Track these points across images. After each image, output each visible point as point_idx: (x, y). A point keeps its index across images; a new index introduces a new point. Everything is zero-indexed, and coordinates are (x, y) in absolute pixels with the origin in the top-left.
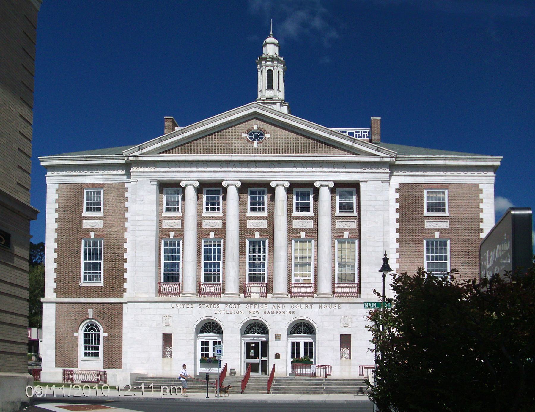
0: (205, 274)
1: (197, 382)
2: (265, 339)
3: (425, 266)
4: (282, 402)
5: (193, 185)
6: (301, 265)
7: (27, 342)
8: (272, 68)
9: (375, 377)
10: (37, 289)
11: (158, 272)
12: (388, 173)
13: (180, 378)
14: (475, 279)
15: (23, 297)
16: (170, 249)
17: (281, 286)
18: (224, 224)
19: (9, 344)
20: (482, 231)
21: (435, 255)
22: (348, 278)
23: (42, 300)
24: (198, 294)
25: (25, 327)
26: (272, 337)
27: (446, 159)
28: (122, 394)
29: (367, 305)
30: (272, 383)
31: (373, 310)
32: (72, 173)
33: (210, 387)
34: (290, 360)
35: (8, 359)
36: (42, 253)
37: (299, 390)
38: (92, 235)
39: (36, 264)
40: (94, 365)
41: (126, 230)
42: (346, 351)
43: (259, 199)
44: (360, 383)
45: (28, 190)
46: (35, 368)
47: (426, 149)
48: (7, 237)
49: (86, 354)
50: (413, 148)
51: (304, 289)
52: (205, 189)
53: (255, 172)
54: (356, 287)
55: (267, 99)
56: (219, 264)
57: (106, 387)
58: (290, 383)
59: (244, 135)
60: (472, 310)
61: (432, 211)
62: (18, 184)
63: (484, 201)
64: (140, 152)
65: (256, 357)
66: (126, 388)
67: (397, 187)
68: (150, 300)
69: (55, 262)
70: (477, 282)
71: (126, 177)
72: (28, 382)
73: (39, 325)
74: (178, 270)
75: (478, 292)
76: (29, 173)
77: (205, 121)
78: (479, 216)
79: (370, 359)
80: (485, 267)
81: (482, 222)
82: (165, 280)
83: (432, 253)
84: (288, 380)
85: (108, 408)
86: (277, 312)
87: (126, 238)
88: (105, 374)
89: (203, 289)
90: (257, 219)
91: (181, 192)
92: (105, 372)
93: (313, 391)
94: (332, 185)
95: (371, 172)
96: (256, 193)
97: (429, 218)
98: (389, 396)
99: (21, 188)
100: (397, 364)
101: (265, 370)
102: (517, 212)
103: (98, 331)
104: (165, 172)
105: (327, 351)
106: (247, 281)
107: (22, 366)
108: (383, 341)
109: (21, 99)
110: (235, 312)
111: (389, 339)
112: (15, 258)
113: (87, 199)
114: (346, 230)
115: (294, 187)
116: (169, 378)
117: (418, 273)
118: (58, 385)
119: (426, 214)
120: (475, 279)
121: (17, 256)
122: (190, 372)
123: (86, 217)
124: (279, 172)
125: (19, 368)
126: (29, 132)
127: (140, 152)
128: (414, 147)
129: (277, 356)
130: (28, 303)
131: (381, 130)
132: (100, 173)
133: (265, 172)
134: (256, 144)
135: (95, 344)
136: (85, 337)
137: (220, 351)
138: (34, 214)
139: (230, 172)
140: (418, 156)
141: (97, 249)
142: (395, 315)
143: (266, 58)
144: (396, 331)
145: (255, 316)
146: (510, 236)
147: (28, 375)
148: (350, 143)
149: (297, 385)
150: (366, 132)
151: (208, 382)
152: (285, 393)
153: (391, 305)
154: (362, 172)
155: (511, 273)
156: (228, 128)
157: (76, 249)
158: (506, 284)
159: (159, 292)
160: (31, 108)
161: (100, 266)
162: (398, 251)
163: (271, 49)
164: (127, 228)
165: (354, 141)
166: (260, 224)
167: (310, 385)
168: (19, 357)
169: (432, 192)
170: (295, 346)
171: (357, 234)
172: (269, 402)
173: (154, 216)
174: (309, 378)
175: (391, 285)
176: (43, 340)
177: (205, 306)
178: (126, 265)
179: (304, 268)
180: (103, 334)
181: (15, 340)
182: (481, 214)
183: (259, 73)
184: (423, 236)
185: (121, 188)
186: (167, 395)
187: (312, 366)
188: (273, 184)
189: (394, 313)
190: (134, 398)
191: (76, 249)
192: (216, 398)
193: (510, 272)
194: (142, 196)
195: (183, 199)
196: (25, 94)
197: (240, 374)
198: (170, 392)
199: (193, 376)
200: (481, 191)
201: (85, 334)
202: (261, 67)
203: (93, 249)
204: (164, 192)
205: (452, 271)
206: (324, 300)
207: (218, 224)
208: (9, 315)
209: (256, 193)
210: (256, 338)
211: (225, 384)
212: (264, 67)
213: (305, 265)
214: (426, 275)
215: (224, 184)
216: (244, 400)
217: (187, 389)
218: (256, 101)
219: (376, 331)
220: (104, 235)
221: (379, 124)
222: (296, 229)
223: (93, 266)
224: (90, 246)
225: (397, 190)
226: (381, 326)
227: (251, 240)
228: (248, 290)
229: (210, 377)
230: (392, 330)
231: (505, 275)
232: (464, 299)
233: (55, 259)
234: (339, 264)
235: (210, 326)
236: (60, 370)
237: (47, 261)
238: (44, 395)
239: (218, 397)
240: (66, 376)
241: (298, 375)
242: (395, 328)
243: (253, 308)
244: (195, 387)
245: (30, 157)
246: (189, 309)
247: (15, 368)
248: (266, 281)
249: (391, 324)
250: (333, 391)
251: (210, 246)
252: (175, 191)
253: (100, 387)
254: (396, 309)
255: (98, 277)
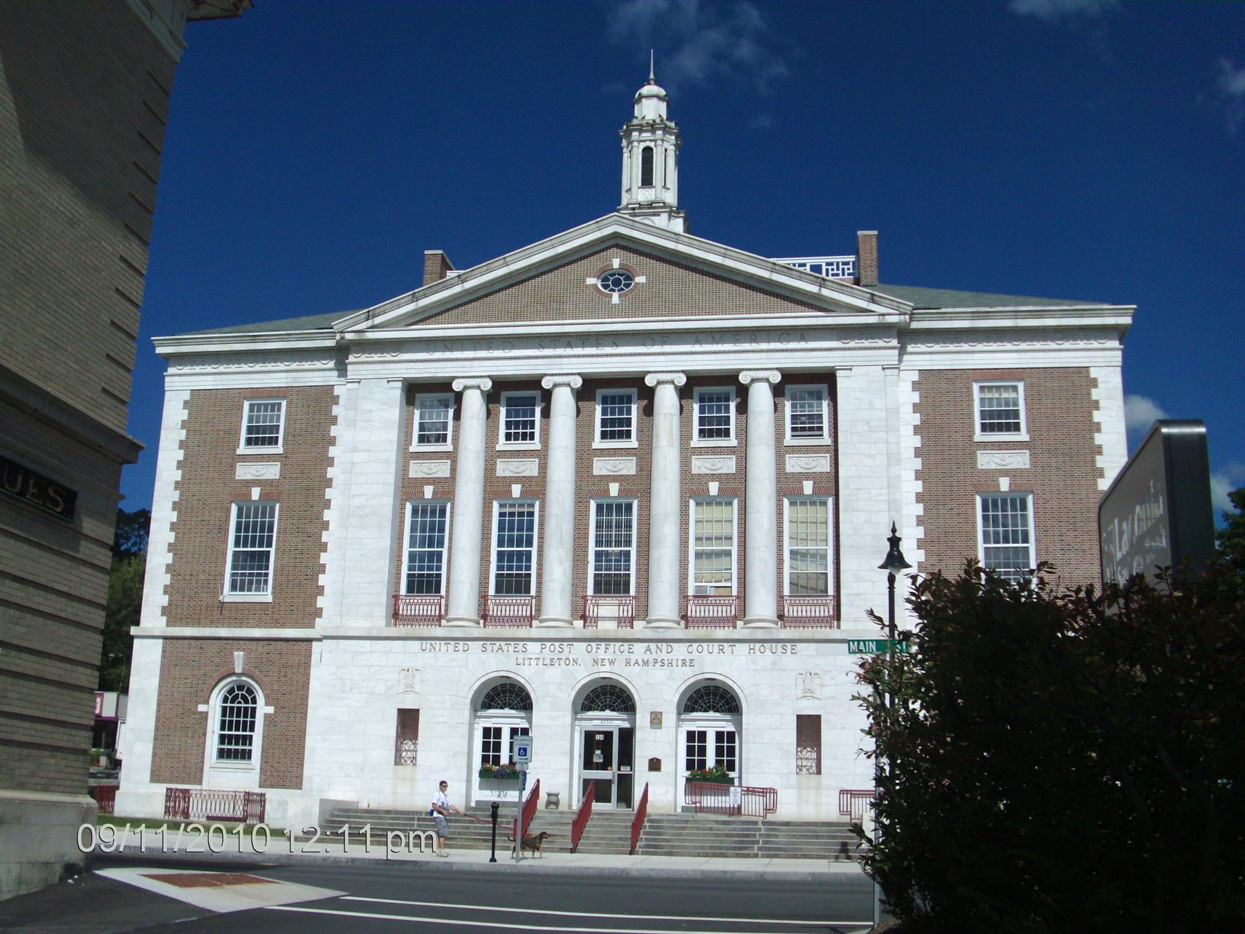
0: (498, 576)
1: (472, 822)
2: (626, 725)
3: (981, 556)
4: (663, 875)
5: (479, 387)
6: (709, 555)
7: (92, 723)
8: (652, 145)
9: (877, 817)
10: (126, 608)
11: (394, 572)
12: (894, 348)
13: (431, 813)
14: (1091, 585)
15: (92, 623)
16: (424, 524)
17: (664, 603)
18: (543, 468)
19: (49, 728)
20: (1101, 473)
21: (1001, 529)
22: (812, 584)
23: (134, 630)
24: (482, 621)
25: (91, 691)
26: (642, 718)
27: (1016, 315)
28: (298, 849)
29: (856, 646)
30: (640, 829)
31: (869, 658)
32: (222, 369)
33: (501, 835)
34: (683, 773)
35: (44, 761)
36: (142, 532)
37: (702, 848)
38: (256, 493)
39: (128, 554)
40: (240, 778)
41: (329, 483)
42: (809, 754)
43: (621, 413)
44: (842, 831)
45: (124, 403)
46: (105, 782)
47: (974, 294)
48: (70, 497)
49: (222, 754)
50: (949, 294)
51: (715, 610)
52: (697, 390)
53: (612, 355)
54: (832, 604)
55: (641, 206)
56: (529, 554)
57: (262, 832)
58: (683, 828)
59: (591, 281)
60: (1088, 660)
61: (992, 430)
62: (104, 390)
63: (1102, 404)
64: (369, 323)
65: (606, 765)
66: (308, 835)
67: (916, 378)
68: (374, 634)
69: (169, 551)
70: (1097, 594)
71: (336, 373)
72: (85, 815)
73: (121, 686)
74: (439, 568)
75: (1100, 615)
76: (129, 370)
77: (510, 256)
78: (1092, 438)
79: (863, 774)
80: (1111, 556)
81: (1100, 453)
82: (410, 589)
83: (996, 524)
84: (677, 821)
85: (263, 881)
86: (656, 661)
87: (329, 501)
88: (262, 799)
89: (493, 610)
90: (615, 455)
91: (452, 401)
92: (263, 795)
93: (735, 848)
94: (776, 378)
95: (860, 349)
96: (613, 399)
97: (985, 445)
98: (910, 864)
99: (108, 398)
100: (926, 787)
101: (625, 797)
102: (1175, 430)
103: (254, 701)
104: (422, 361)
105: (767, 756)
106: (590, 591)
107: (74, 777)
108: (893, 732)
109: (127, 226)
110: (562, 662)
111: (905, 727)
112: (83, 542)
113: (250, 420)
114: (807, 476)
115: (694, 386)
116: (408, 813)
117: (966, 572)
118: (153, 824)
119: (979, 436)
120: (1091, 585)
121: (88, 538)
122: (455, 799)
123: (245, 458)
124: (663, 354)
125: (68, 783)
126: (136, 289)
127: (369, 323)
128: (950, 292)
129: (655, 765)
130: (101, 638)
131: (880, 258)
132: (281, 366)
133: (635, 355)
134: (616, 298)
135: (244, 730)
136: (224, 715)
137: (525, 750)
138: (136, 452)
139: (560, 357)
140: (957, 310)
141: (263, 523)
142: (919, 671)
143: (641, 125)
144: (922, 707)
145: (605, 671)
146: (1162, 484)
147: (87, 800)
148: (813, 289)
149: (698, 835)
150: (847, 263)
151: (494, 822)
152: (670, 854)
153: (908, 646)
154: (840, 349)
155: (1170, 572)
156: (558, 268)
157: (217, 522)
158: (1161, 597)
159: (396, 615)
160: (144, 242)
161: (268, 560)
162: (920, 521)
163: (651, 106)
164: (331, 480)
165: (823, 283)
166: (622, 466)
167: (727, 835)
168: (71, 757)
169: (990, 388)
170: (696, 740)
171: (830, 485)
172: (635, 873)
173: (391, 454)
174: (726, 818)
175: (908, 601)
176: (129, 719)
177: (496, 648)
178: (324, 558)
179: (716, 563)
180: (263, 709)
181: (64, 718)
182: (1096, 435)
183: (626, 156)
184: (975, 486)
185: (326, 396)
186: (402, 853)
187: (732, 789)
188: (650, 381)
189: (915, 666)
190: (324, 859)
191: (217, 522)
192: (513, 862)
193: (1167, 568)
194: (370, 411)
195: (457, 416)
196: (133, 215)
197: (570, 806)
198: (408, 845)
199: (462, 809)
200: (1094, 383)
201: (224, 709)
202: (630, 143)
203: (255, 523)
204: (417, 402)
205: (1041, 565)
206: (759, 635)
207: (530, 468)
208: (58, 664)
209: (613, 399)
210: (608, 721)
211: (535, 829)
212: (635, 144)
213: (719, 554)
214: (983, 575)
215: (546, 383)
216: (576, 868)
217: (446, 838)
218: (618, 211)
219: (875, 708)
220: (280, 494)
221: (874, 244)
222: (700, 475)
223: (253, 560)
224: (248, 516)
225: (916, 386)
226: (887, 695)
227: (600, 501)
228: (591, 611)
229: (501, 811)
230: (911, 707)
231: (1158, 576)
232: (1071, 634)
233: (170, 545)
234: (792, 553)
235: (506, 694)
236: (161, 789)
237: (151, 549)
238: (118, 847)
239: (518, 859)
240: (172, 804)
241: (702, 810)
242: (919, 701)
243: (601, 651)
244: (465, 834)
245: (133, 338)
246: (461, 655)
247: (58, 782)
248: (633, 592)
249: (910, 691)
250: (780, 849)
251: (512, 514)
252: (439, 401)
253: (248, 831)
254: (920, 657)
255: (260, 583)
